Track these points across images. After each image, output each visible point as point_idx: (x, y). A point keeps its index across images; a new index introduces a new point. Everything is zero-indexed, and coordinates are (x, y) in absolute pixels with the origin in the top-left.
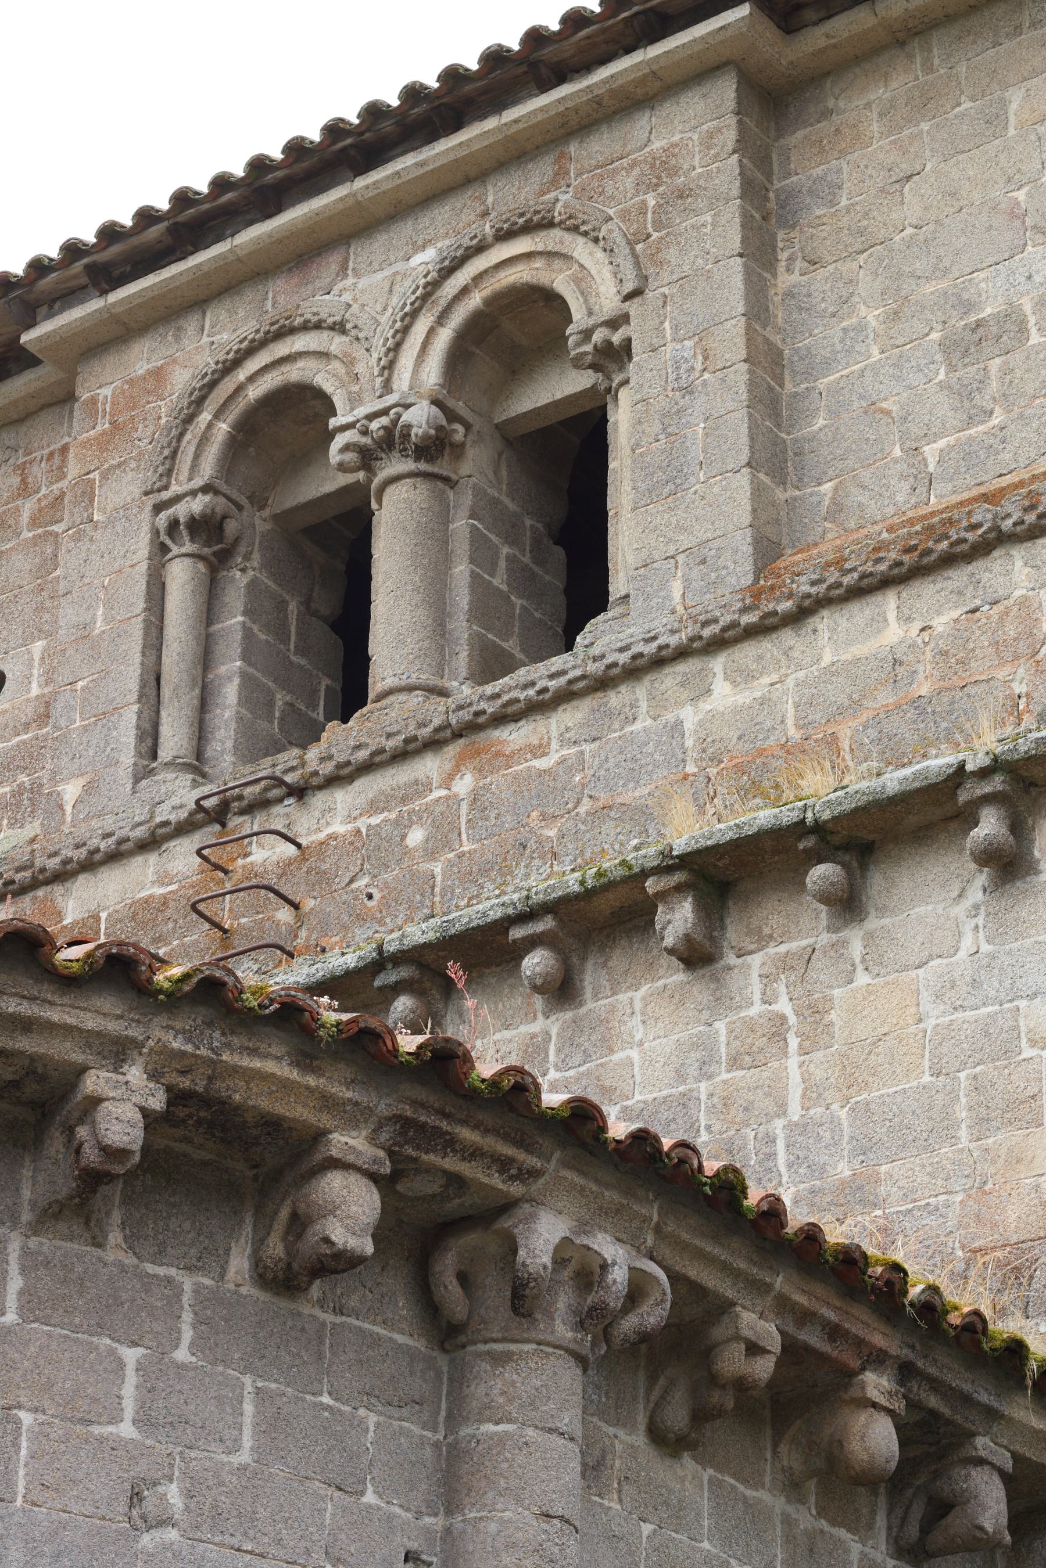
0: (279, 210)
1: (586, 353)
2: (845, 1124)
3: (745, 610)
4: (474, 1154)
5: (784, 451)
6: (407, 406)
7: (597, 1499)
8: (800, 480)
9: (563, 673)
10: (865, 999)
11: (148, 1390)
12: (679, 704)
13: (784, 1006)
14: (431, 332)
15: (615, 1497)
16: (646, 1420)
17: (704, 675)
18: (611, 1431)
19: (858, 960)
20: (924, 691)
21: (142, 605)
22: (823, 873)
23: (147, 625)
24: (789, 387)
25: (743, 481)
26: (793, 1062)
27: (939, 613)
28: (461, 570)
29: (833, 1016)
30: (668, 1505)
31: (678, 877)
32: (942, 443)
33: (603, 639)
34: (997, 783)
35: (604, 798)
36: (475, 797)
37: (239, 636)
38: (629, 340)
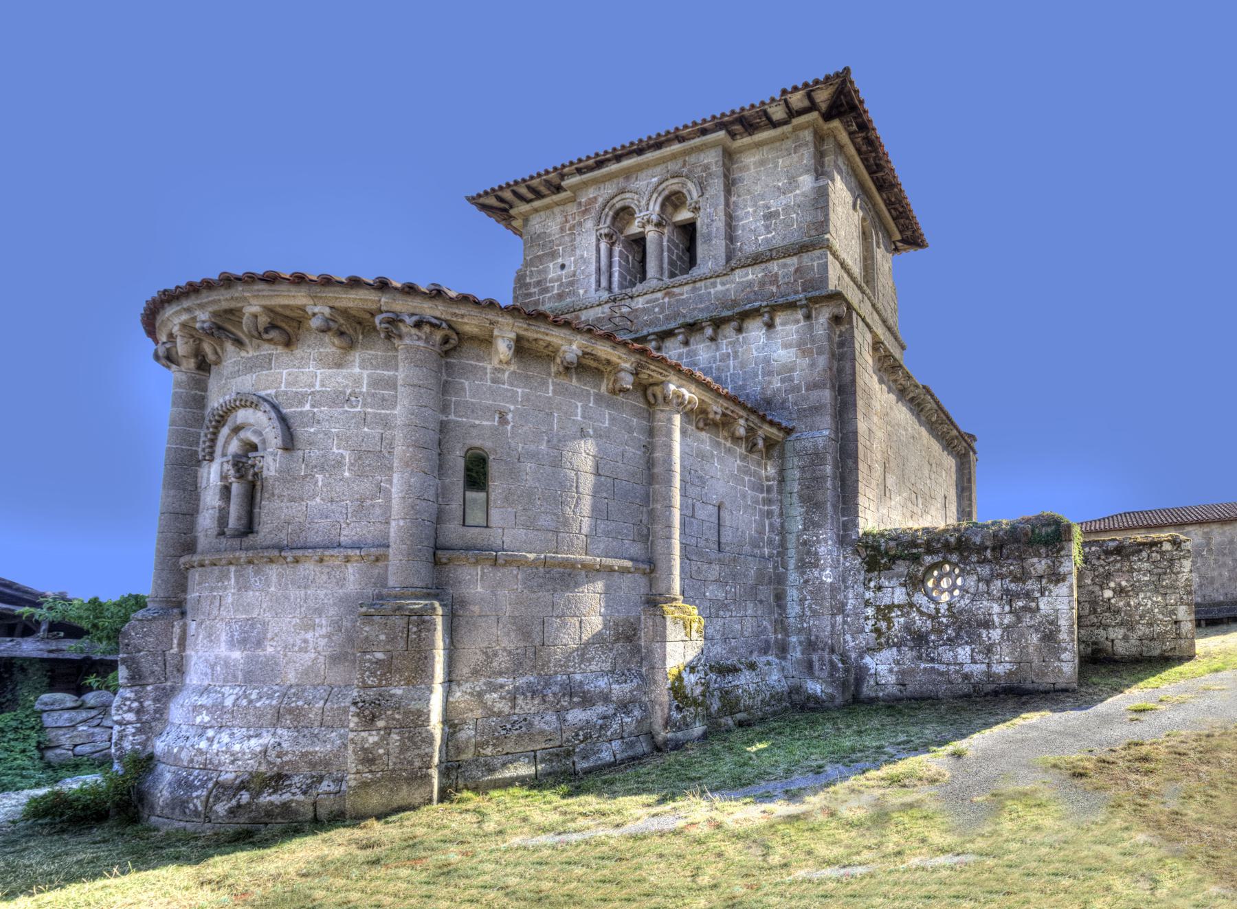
11: (584, 412)
22: (734, 324)
25: (723, 242)
28: (666, 254)
33: (696, 272)
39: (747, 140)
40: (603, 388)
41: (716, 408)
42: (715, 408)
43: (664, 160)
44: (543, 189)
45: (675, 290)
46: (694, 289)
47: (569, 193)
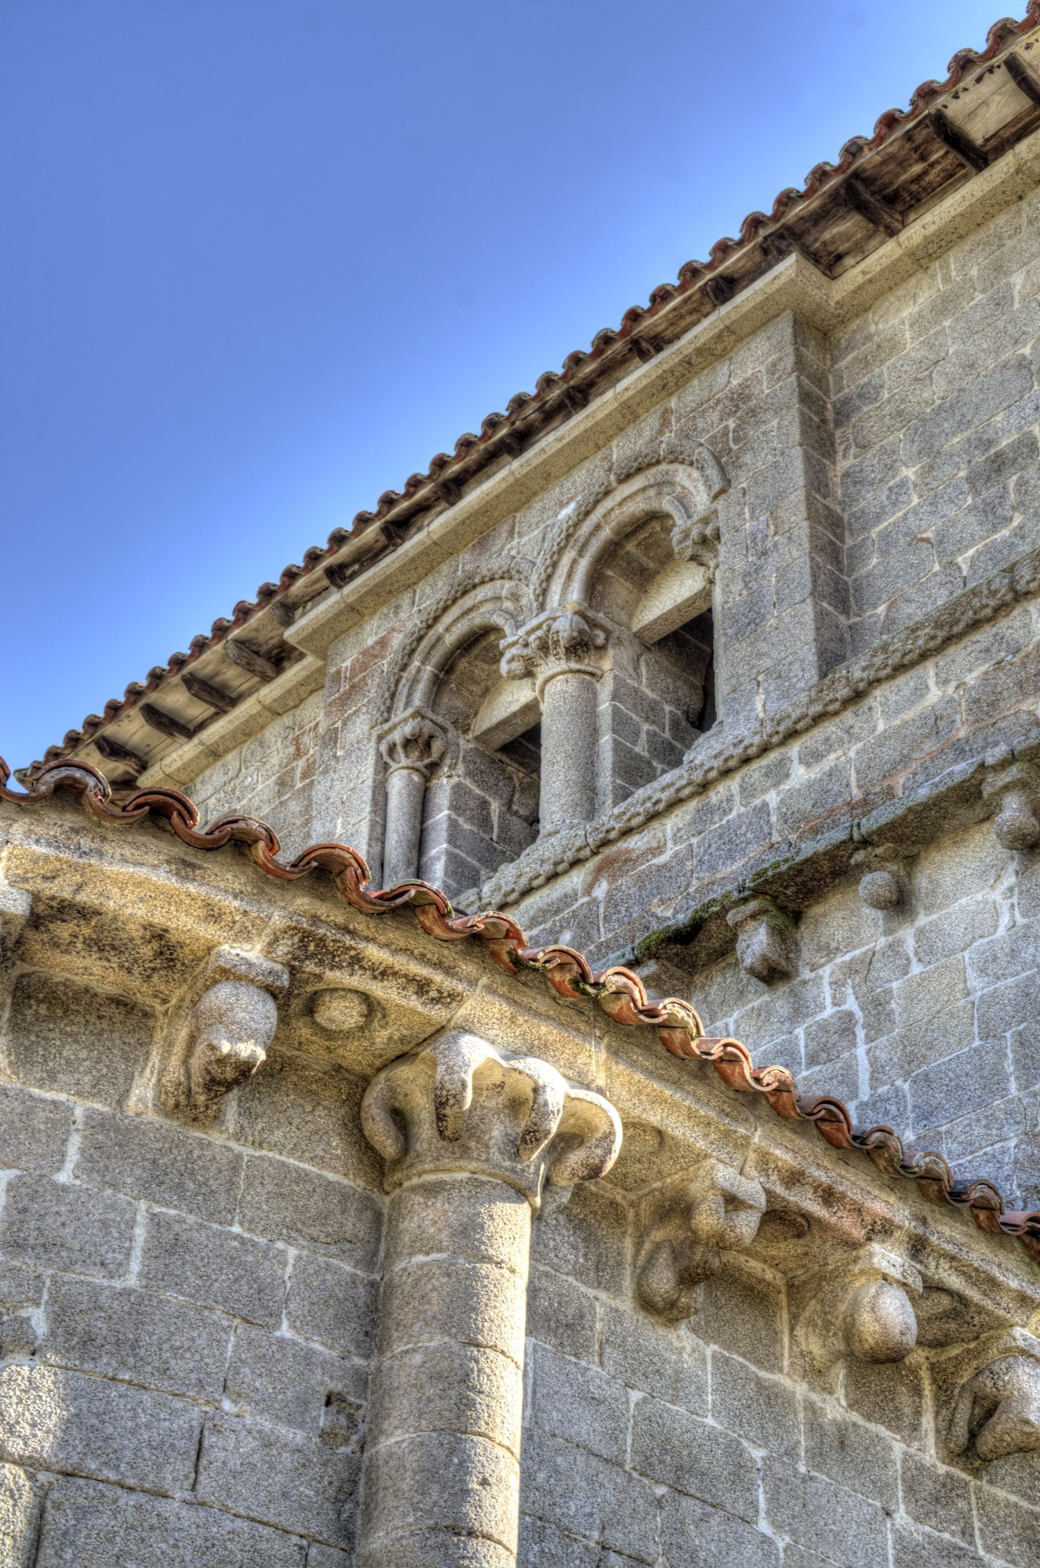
0: (460, 497)
1: (687, 547)
2: (908, 1096)
3: (812, 702)
4: (384, 974)
5: (847, 590)
6: (554, 619)
7: (573, 1359)
8: (861, 609)
9: (672, 784)
10: (919, 985)
12: (764, 791)
13: (851, 1004)
14: (574, 562)
15: (596, 1359)
16: (634, 1286)
17: (783, 764)
18: (591, 1292)
19: (911, 955)
20: (962, 734)
21: (368, 809)
23: (373, 825)
24: (849, 542)
26: (861, 1051)
27: (970, 670)
28: (606, 740)
29: (893, 1005)
30: (661, 1375)
31: (753, 905)
32: (971, 552)
34: (1014, 772)
35: (707, 876)
36: (610, 896)
37: (445, 826)
38: (718, 529)
39: (886, 253)
40: (143, 1093)
41: (734, 1169)
42: (725, 1175)
43: (596, 440)
44: (233, 676)
45: (635, 843)
46: (706, 814)
47: (310, 662)
